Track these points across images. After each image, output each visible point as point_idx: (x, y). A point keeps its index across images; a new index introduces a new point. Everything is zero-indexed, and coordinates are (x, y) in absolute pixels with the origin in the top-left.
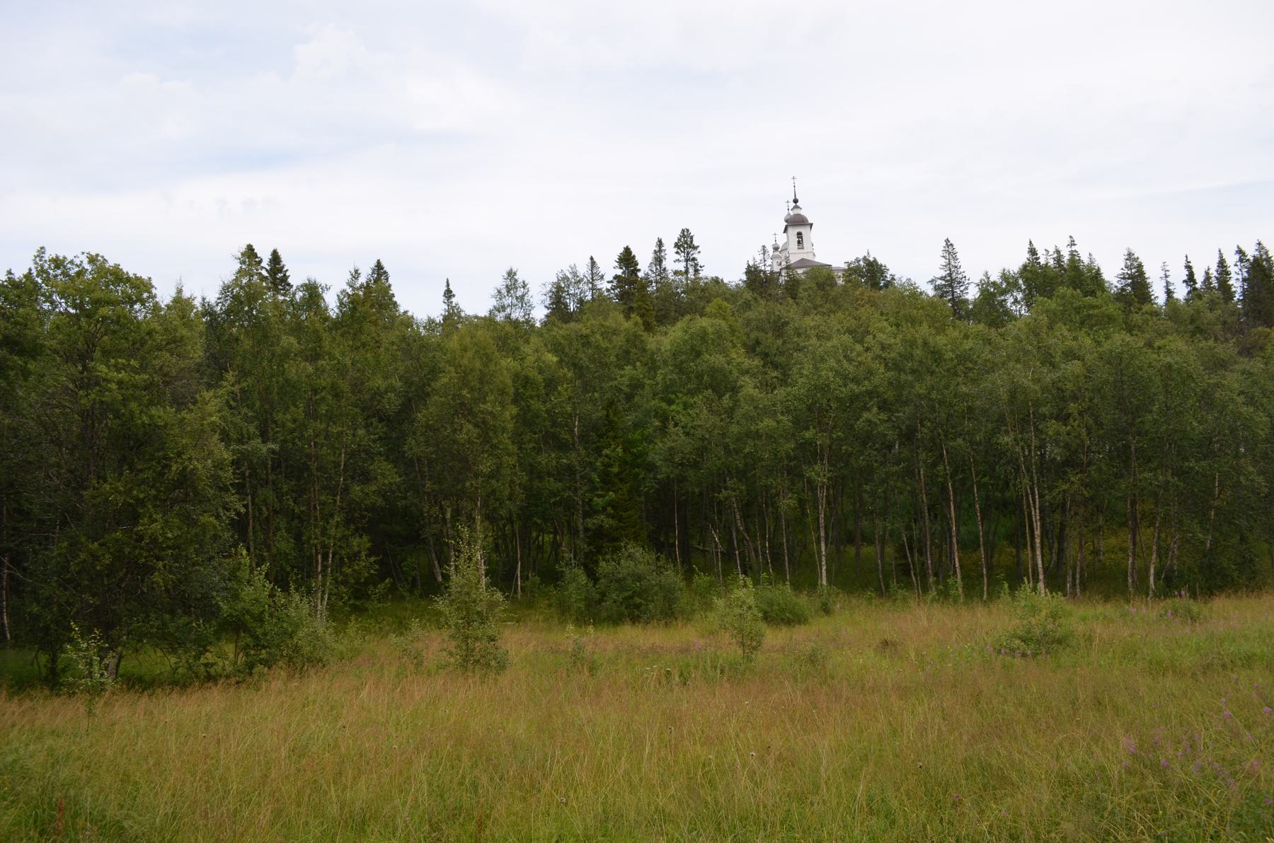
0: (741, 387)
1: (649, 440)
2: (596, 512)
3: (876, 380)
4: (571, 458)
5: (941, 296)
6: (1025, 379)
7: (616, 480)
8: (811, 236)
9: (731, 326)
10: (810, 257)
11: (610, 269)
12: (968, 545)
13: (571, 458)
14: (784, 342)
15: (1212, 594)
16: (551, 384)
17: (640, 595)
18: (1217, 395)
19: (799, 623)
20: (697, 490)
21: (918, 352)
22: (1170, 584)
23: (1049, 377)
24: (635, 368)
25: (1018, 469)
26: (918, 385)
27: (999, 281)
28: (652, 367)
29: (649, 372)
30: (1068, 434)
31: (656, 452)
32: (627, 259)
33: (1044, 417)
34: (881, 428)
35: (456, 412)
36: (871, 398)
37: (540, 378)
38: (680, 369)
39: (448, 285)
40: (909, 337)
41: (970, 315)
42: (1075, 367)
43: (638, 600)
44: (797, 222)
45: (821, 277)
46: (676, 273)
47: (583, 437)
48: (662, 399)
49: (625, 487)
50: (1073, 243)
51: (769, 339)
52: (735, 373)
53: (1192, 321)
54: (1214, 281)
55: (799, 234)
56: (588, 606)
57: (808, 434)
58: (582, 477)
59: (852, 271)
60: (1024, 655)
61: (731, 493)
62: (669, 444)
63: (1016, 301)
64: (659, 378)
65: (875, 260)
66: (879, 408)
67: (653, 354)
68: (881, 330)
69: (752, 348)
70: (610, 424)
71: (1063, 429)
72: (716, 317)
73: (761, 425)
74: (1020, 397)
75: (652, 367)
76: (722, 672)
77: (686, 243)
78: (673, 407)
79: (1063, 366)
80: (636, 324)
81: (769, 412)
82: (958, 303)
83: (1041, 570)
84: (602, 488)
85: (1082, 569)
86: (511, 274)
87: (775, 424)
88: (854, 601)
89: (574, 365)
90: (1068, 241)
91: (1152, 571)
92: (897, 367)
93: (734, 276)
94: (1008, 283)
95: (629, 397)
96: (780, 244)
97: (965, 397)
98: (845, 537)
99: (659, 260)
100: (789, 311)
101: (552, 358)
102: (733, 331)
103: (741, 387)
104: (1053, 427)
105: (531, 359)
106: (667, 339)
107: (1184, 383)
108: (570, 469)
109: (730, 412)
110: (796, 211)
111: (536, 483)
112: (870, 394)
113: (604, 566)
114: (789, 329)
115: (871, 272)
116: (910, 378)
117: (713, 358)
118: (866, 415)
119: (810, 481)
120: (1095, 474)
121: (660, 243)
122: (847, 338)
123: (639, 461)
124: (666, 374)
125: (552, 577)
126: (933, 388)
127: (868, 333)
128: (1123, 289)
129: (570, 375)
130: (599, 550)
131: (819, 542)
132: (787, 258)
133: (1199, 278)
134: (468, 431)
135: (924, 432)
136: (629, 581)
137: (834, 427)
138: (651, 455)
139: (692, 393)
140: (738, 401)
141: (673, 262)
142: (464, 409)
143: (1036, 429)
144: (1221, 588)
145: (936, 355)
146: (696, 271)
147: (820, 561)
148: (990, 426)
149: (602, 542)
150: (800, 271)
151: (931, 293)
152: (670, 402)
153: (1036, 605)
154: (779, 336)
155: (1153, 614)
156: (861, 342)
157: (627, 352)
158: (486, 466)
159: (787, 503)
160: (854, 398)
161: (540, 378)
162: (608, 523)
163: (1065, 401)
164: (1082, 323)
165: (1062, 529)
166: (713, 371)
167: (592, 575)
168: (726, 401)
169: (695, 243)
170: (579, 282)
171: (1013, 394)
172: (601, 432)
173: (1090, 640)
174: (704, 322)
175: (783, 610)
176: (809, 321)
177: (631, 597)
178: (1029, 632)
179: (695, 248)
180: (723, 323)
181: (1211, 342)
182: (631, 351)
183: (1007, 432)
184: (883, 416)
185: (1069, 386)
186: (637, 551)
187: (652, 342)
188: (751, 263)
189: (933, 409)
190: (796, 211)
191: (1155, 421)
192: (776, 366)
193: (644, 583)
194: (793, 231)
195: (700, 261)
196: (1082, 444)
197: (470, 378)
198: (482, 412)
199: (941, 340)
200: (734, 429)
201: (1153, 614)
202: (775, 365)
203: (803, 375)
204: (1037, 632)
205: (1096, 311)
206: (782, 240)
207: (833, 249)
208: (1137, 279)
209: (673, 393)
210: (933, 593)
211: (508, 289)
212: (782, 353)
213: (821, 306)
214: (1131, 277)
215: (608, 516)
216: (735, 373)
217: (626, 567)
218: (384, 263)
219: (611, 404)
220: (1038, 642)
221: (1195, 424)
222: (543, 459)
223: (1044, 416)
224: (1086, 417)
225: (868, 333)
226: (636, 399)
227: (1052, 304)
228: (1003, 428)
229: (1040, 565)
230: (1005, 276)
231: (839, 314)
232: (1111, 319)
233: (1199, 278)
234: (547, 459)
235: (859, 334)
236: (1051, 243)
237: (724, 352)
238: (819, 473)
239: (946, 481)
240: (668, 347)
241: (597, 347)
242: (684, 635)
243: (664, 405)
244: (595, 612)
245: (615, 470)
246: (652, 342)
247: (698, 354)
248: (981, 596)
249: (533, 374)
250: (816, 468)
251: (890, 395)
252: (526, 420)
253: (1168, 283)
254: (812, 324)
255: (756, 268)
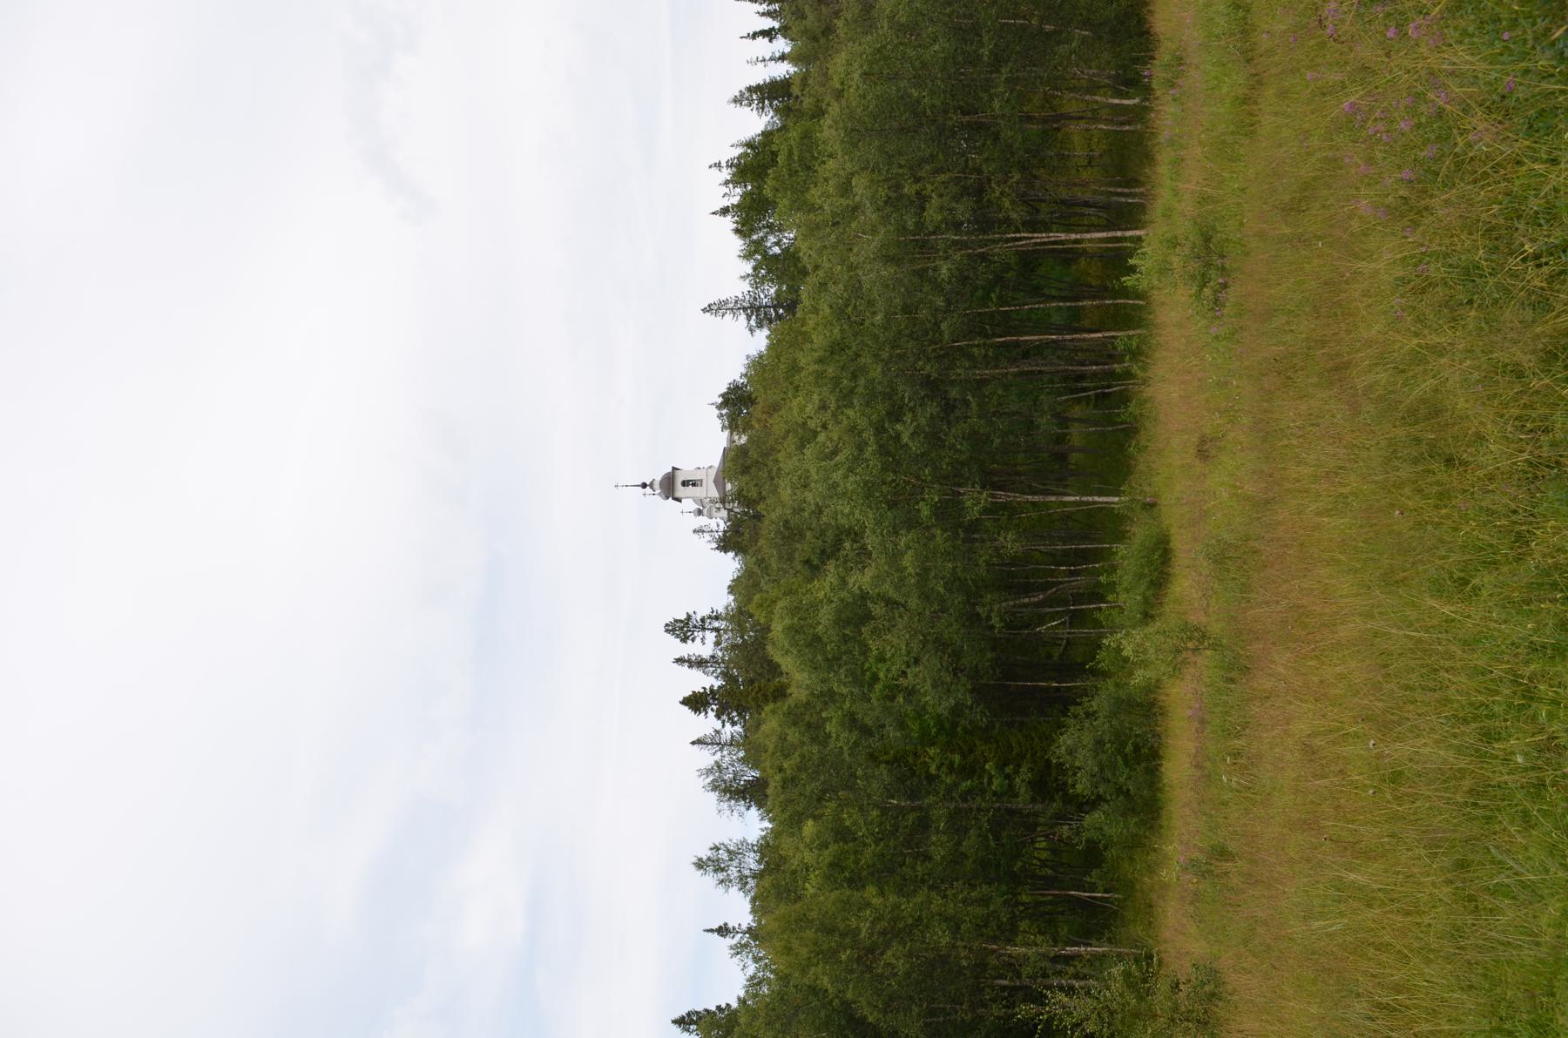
0: (860, 588)
1: (920, 713)
2: (1011, 786)
3: (862, 423)
4: (940, 814)
5: (771, 321)
6: (869, 245)
7: (972, 757)
8: (687, 469)
10: (713, 473)
11: (707, 723)
12: (1073, 322)
13: (940, 814)
15: (1147, 32)
16: (843, 834)
17: (1123, 745)
18: (903, 20)
19: (1168, 542)
20: (989, 655)
21: (831, 370)
22: (1131, 80)
23: (870, 215)
24: (829, 719)
25: (983, 257)
26: (872, 374)
27: (753, 263)
28: (830, 697)
29: (834, 702)
30: (941, 196)
31: (937, 703)
32: (696, 702)
33: (920, 226)
34: (923, 421)
35: (870, 969)
36: (886, 431)
37: (833, 848)
38: (833, 662)
39: (711, 931)
40: (811, 379)
41: (794, 290)
42: (860, 185)
43: (1129, 748)
44: (669, 486)
45: (737, 463)
46: (717, 644)
47: (913, 795)
48: (871, 686)
49: (981, 747)
50: (718, 165)
51: (803, 549)
53: (815, 39)
54: (772, 7)
55: (684, 484)
56: (1134, 811)
57: (925, 511)
58: (965, 800)
59: (733, 424)
60: (1225, 286)
61: (995, 609)
62: (928, 686)
63: (777, 244)
64: (845, 691)
65: (722, 395)
67: (812, 694)
68: (802, 409)
69: (814, 568)
70: (898, 760)
71: (935, 201)
72: (772, 612)
73: (911, 570)
74: (893, 251)
75: (830, 697)
76: (1232, 681)
77: (682, 629)
78: (881, 675)
79: (857, 199)
80: (773, 712)
81: (895, 557)
82: (778, 302)
83: (1111, 234)
84: (980, 777)
85: (1109, 185)
86: (700, 865)
87: (910, 552)
88: (1141, 467)
89: (819, 800)
90: (715, 170)
91: (1116, 101)
92: (846, 398)
93: (729, 565)
94: (756, 252)
95: (866, 731)
97: (889, 317)
98: (1056, 466)
99: (700, 663)
100: (773, 515)
101: (809, 827)
102: (790, 592)
103: (860, 588)
104: (932, 214)
105: (809, 857)
106: (800, 679)
107: (886, 58)
108: (954, 816)
109: (890, 603)
110: (657, 486)
111: (969, 865)
112: (879, 430)
113: (1082, 786)
114: (795, 520)
115: (736, 403)
116: (862, 382)
118: (905, 439)
119: (986, 511)
120: (992, 167)
121: (680, 661)
122: (809, 452)
123: (947, 726)
124: (840, 681)
125: (1093, 855)
126: (876, 356)
127: (804, 424)
128: (777, 110)
129: (833, 805)
130: (1063, 787)
131: (1065, 504)
132: (712, 501)
133: (768, 23)
134: (895, 958)
135: (930, 369)
136: (1103, 757)
137: (918, 478)
138: (940, 710)
139: (865, 650)
141: (704, 646)
142: (868, 955)
143: (934, 233)
144: (1141, 21)
145: (836, 348)
146: (717, 618)
147: (1089, 503)
148: (926, 288)
149: (1049, 782)
150: (729, 487)
151: (766, 332)
152: (875, 678)
153: (1158, 258)
154: (802, 535)
155: (1171, 109)
156: (815, 434)
157: (809, 725)
158: (941, 937)
159: (1011, 543)
160: (883, 451)
161: (833, 848)
162: (1025, 774)
163: (901, 196)
164: (809, 168)
165: (1063, 202)
166: (840, 621)
167: (1094, 803)
168: (878, 610)
169: (683, 617)
170: (719, 766)
171: (888, 259)
172: (908, 773)
173: (1204, 199)
174: (777, 628)
175: (1151, 563)
176: (786, 493)
177: (1125, 757)
178: (1193, 277)
179: (689, 617)
180: (780, 604)
181: (839, 23)
182: (808, 721)
183: (935, 269)
184: (908, 418)
185: (882, 192)
186: (1066, 740)
187: (798, 694)
189: (901, 357)
190: (657, 486)
191: (933, 93)
192: (837, 545)
193: (1106, 738)
194: (681, 491)
195: (706, 612)
196: (957, 180)
197: (825, 947)
198: (871, 934)
199: (819, 340)
200: (914, 602)
201: (1171, 109)
202: (836, 545)
203: (845, 512)
204: (1194, 266)
205: (796, 152)
206: (689, 505)
207: (705, 444)
208: (766, 93)
209: (863, 672)
210: (1135, 369)
211: (719, 869)
212: (823, 533)
213: (770, 472)
214: (761, 100)
215: (1017, 772)
216: (844, 594)
217: (1085, 760)
218: (677, 1016)
219: (873, 758)
220: (1208, 265)
221: (936, 48)
222: (938, 853)
223: (916, 224)
224: (922, 174)
225: (804, 424)
226: (868, 721)
227: (783, 203)
228: (930, 273)
229: (1104, 235)
230: (747, 256)
231: (780, 456)
232: (806, 135)
233: (768, 23)
234: (938, 846)
235: (806, 437)
236: (718, 191)
237: (815, 606)
238: (975, 500)
239: (991, 346)
240: (805, 675)
241: (799, 769)
242: (1184, 699)
243: (878, 687)
244: (1146, 808)
245: (957, 758)
246: (798, 694)
247: (817, 638)
248: (1140, 308)
249: (828, 855)
250: (968, 504)
251: (882, 407)
252: (885, 872)
253: (771, 59)
254: (789, 491)
255: (721, 540)
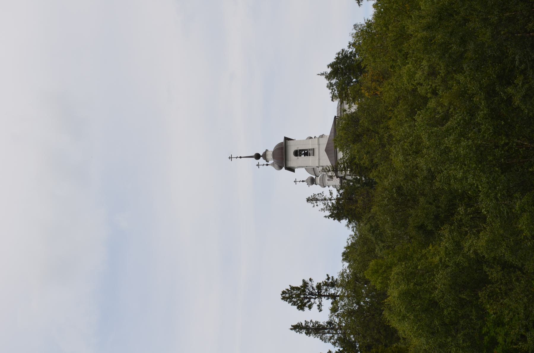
8: (300, 137)
9: (400, 260)
10: (324, 142)
14: (423, 194)
21: (439, 37)
45: (347, 131)
46: (334, 310)
52: (459, 259)
55: (297, 153)
59: (342, 93)
65: (331, 65)
66: (509, 84)
68: (411, 76)
69: (428, 234)
77: (299, 296)
78: (500, 339)
87: (525, 216)
93: (343, 232)
96: (307, 175)
109: (506, 266)
110: (270, 156)
116: (471, 46)
117: (438, 286)
118: (517, 101)
121: (297, 328)
127: (414, 90)
132: (325, 170)
140: (494, 258)
141: (321, 313)
146: (333, 284)
150: (340, 155)
156: (426, 100)
169: (299, 284)
179: (305, 284)
184: (519, 80)
188: (328, 213)
190: (270, 156)
194: (293, 161)
206: (302, 174)
207: (316, 114)
213: (381, 139)
216: (459, 259)
225: (414, 90)
247: (434, 303)
254: (401, 158)
